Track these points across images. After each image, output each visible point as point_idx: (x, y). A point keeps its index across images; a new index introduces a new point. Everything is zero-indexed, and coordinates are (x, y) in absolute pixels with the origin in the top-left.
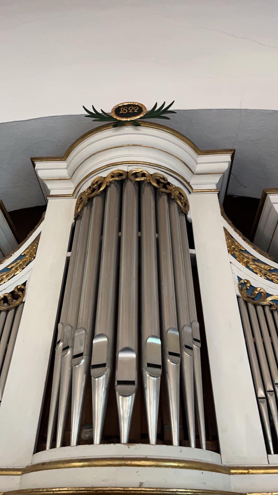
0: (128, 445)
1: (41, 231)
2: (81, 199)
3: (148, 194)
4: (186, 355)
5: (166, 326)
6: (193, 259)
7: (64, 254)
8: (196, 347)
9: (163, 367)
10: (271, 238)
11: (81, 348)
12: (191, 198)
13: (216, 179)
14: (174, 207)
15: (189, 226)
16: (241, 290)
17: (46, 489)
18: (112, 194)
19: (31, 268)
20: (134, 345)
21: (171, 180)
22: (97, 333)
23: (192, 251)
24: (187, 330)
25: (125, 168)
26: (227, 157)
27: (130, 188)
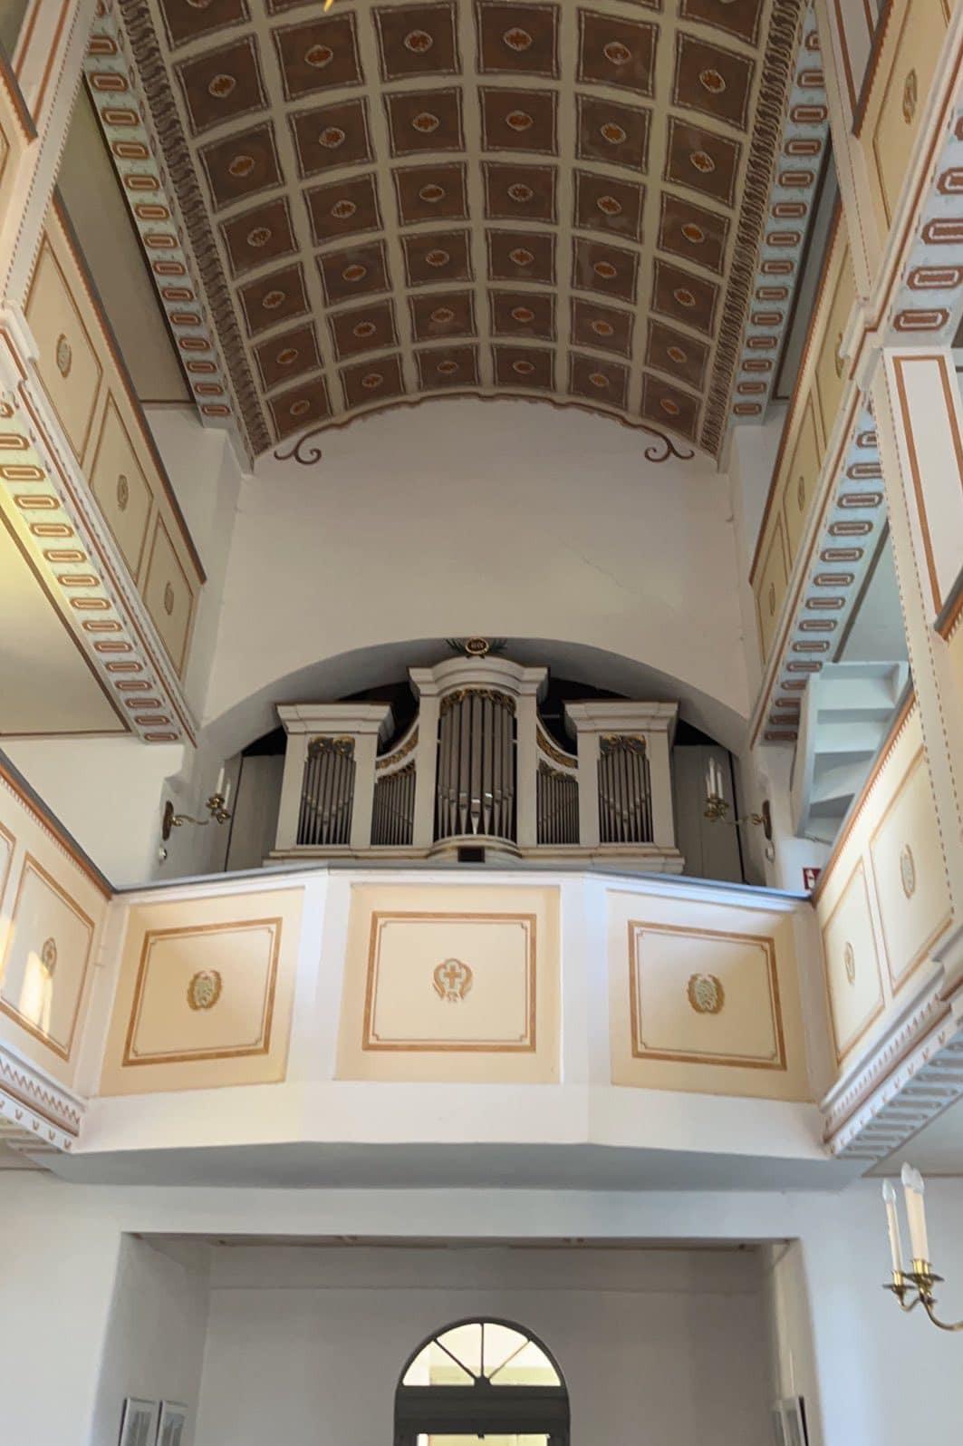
0: (672, 719)
3: (488, 705)
4: (504, 802)
5: (495, 787)
6: (515, 747)
7: (436, 740)
8: (510, 799)
9: (493, 807)
10: (876, 319)
11: (453, 797)
12: (518, 700)
13: (536, 686)
15: (515, 721)
16: (540, 767)
18: (466, 703)
19: (57, 337)
20: (479, 796)
21: (504, 691)
22: (152, 412)
23: (515, 741)
24: (506, 790)
25: (473, 686)
26: (545, 671)
27: (477, 702)
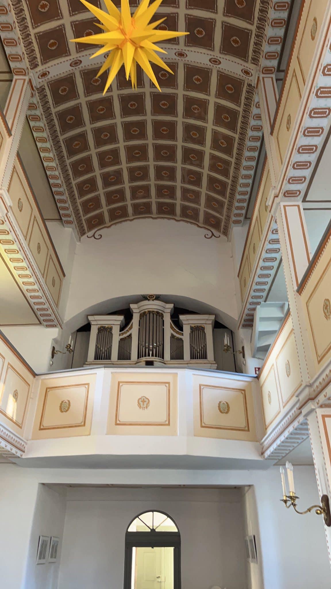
1: (53, 277)
2: (141, 315)
3: (155, 316)
4: (160, 347)
5: (157, 342)
6: (163, 329)
7: (138, 327)
8: (162, 345)
11: (144, 345)
13: (170, 310)
14: (160, 318)
15: (163, 321)
17: (73, 350)
18: (148, 315)
21: (160, 311)
24: (160, 343)
25: (150, 310)
26: (173, 305)
27: (151, 315)
